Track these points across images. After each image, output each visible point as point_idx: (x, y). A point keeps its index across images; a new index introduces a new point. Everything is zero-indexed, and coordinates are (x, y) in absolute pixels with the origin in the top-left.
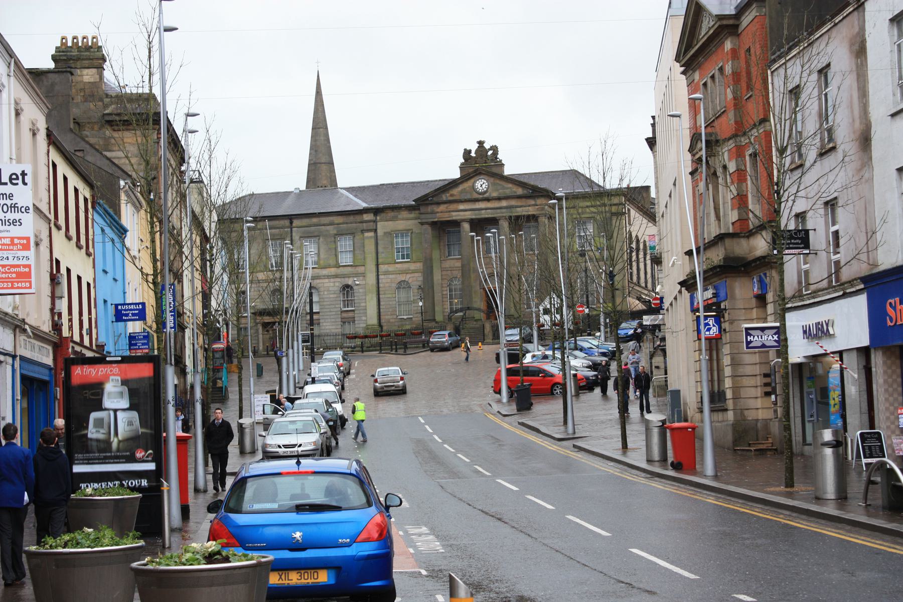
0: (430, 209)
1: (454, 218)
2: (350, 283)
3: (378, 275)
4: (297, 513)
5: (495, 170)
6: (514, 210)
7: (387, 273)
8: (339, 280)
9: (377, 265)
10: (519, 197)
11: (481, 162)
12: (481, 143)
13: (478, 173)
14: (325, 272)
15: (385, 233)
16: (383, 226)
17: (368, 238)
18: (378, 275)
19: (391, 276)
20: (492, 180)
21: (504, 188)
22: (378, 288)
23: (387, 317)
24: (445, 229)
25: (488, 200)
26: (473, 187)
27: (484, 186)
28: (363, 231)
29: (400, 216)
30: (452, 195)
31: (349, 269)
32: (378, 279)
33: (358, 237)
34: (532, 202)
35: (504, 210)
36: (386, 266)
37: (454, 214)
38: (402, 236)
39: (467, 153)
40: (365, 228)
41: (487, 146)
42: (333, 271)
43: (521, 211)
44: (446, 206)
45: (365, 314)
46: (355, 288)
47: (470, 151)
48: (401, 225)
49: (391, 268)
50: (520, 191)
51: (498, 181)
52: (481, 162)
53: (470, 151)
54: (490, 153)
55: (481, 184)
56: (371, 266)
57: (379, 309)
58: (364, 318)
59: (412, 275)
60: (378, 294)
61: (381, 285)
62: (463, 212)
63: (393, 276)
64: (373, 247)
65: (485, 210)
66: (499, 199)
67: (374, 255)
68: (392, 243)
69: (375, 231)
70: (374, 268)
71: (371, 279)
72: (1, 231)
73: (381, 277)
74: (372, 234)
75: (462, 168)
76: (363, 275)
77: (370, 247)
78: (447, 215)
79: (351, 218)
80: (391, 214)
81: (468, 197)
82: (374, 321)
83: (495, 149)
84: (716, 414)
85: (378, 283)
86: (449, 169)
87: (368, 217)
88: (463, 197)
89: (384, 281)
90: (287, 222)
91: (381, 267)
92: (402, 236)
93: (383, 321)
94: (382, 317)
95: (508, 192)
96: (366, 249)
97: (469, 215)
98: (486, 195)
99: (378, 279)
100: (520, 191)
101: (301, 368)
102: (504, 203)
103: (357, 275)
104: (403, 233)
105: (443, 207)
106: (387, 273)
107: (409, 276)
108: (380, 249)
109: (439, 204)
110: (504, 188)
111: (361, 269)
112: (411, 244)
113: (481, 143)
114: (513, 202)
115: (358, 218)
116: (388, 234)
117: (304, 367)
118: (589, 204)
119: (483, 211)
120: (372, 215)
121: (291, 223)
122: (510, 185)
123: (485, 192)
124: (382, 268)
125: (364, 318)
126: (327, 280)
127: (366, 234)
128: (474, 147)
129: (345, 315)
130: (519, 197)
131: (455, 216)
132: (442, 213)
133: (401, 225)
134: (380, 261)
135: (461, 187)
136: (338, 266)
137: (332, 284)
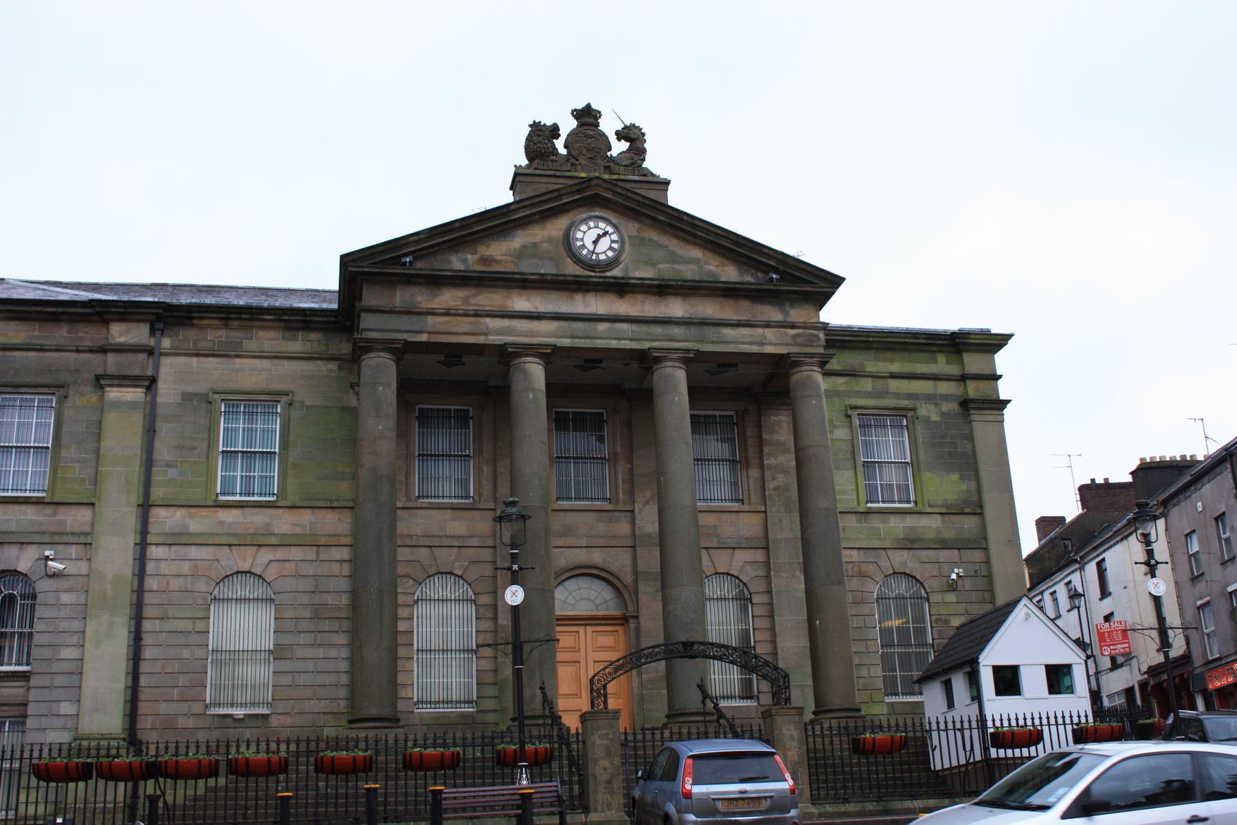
0: (401, 297)
1: (493, 339)
2: (23, 566)
3: (143, 545)
6: (710, 332)
7: (178, 539)
9: (145, 507)
10: (730, 292)
11: (582, 170)
12: (587, 117)
15: (187, 397)
16: (178, 374)
17: (117, 405)
18: (143, 545)
19: (194, 552)
20: (631, 227)
21: (673, 258)
22: (140, 591)
23: (164, 708)
24: (456, 392)
25: (621, 288)
26: (567, 240)
27: (604, 244)
28: (100, 381)
29: (250, 345)
31: (29, 513)
32: (142, 560)
33: (82, 400)
34: (773, 314)
35: (677, 331)
36: (179, 513)
37: (493, 323)
38: (250, 414)
39: (540, 138)
40: (111, 370)
41: (609, 126)
43: (740, 341)
44: (461, 293)
45: (76, 692)
46: (43, 586)
48: (250, 373)
49: (198, 523)
50: (730, 273)
51: (653, 235)
53: (554, 131)
54: (619, 147)
55: (596, 238)
56: (119, 507)
57: (135, 674)
58: (66, 708)
59: (280, 554)
60: (138, 618)
61: (151, 583)
62: (527, 322)
64: (135, 441)
65: (608, 322)
66: (661, 289)
67: (136, 468)
68: (211, 431)
69: (151, 384)
70: (130, 518)
71: (115, 555)
72: (114, 823)
73: (154, 552)
74: (135, 394)
75: (519, 179)
76: (85, 541)
77: (122, 438)
78: (464, 324)
79: (62, 333)
80: (216, 335)
81: (547, 269)
83: (632, 135)
85: (141, 574)
86: (549, 123)
88: (528, 267)
89: (165, 568)
92: (250, 414)
93: (144, 722)
94: (143, 708)
95: (689, 272)
96: (105, 443)
97: (546, 333)
98: (616, 272)
99: (142, 560)
100: (730, 273)
102: (676, 308)
103: (57, 538)
104: (254, 402)
105: (449, 298)
106: (178, 539)
107: (265, 556)
108: (162, 452)
109: (437, 281)
110: (673, 258)
111: (77, 518)
112: (284, 444)
113: (587, 117)
114: (709, 309)
115: (89, 335)
116: (202, 402)
118: (895, 367)
119: (602, 327)
120: (145, 329)
122: (696, 253)
123: (611, 263)
124: (165, 519)
125: (66, 708)
127: (113, 394)
130: (730, 292)
131: (497, 332)
132: (447, 317)
133: (250, 373)
134: (157, 493)
135: (519, 240)
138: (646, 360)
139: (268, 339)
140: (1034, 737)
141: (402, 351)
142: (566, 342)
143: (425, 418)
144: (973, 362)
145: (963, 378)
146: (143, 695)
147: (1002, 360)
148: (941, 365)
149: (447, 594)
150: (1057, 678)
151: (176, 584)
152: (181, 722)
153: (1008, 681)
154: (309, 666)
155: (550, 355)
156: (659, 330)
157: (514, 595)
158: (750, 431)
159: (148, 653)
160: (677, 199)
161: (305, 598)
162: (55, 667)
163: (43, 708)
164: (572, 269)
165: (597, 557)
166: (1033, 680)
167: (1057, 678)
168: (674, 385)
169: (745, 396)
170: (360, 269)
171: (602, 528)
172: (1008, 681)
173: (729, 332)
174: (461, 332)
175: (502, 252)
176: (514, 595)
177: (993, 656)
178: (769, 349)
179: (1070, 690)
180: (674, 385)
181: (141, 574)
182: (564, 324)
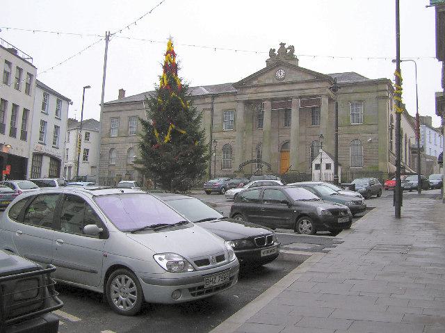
5: (292, 62)
10: (307, 82)
11: (283, 58)
12: (282, 45)
25: (284, 84)
39: (272, 51)
41: (286, 46)
43: (308, 92)
47: (274, 50)
50: (309, 78)
52: (283, 58)
55: (281, 74)
65: (281, 92)
83: (292, 48)
88: (267, 82)
98: (284, 81)
113: (282, 45)
123: (284, 78)
128: (277, 48)
130: (307, 82)
169: (311, 108)
173: (306, 91)
175: (264, 80)
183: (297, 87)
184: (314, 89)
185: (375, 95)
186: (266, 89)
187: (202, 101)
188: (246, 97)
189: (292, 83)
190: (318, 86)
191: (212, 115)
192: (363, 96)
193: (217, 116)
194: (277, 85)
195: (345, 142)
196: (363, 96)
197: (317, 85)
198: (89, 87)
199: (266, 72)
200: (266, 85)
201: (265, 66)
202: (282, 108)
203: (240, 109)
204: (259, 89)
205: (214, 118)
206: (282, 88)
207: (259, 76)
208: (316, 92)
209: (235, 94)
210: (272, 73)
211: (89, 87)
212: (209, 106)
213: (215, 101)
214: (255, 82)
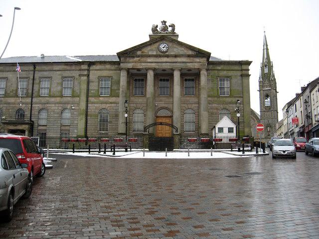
4: (210, 54)
5: (174, 38)
7: (93, 103)
8: (62, 105)
10: (189, 56)
11: (163, 36)
13: (162, 39)
14: (53, 100)
19: (96, 105)
22: (87, 112)
25: (168, 56)
27: (165, 49)
30: (142, 52)
31: (69, 98)
32: (87, 107)
39: (155, 29)
41: (168, 24)
42: (58, 99)
43: (190, 66)
47: (157, 26)
48: (105, 73)
50: (190, 52)
52: (163, 36)
55: (163, 47)
61: (89, 110)
62: (150, 63)
63: (98, 105)
65: (165, 64)
73: (89, 105)
74: (85, 78)
81: (155, 53)
82: (83, 134)
83: (173, 26)
84: (34, 133)
85: (87, 109)
87: (85, 67)
88: (150, 53)
90: (32, 68)
91: (90, 98)
95: (181, 53)
98: (167, 53)
99: (87, 107)
100: (190, 52)
101: (230, 150)
106: (93, 103)
107: (108, 105)
114: (184, 59)
117: (230, 148)
121: (35, 68)
123: (166, 52)
124: (91, 99)
126: (53, 105)
127: (82, 78)
128: (160, 26)
129: (63, 128)
130: (189, 56)
134: (90, 95)
136: (62, 96)
137: (56, 108)
138: (173, 70)
139: (108, 66)
140: (221, 140)
141: (128, 70)
142: (157, 67)
143: (186, 80)
144: (244, 67)
145: (242, 70)
146: (88, 129)
147: (250, 67)
148: (237, 67)
149: (139, 112)
150: (230, 130)
151: (93, 110)
152: (94, 134)
153: (221, 130)
154: (115, 124)
155: (154, 70)
156: (174, 64)
157: (126, 115)
158: (197, 82)
159: (88, 122)
160: (180, 39)
161: (114, 113)
162: (74, 124)
163: (72, 131)
164: (159, 53)
165: (166, 106)
166: (226, 130)
167: (230, 130)
168: (150, 75)
169: (190, 77)
170: (121, 55)
171: (167, 100)
172: (221, 130)
173: (188, 64)
174: (139, 66)
175: (146, 50)
176: (126, 115)
177: (218, 126)
178: (196, 67)
179: (233, 132)
180: (150, 75)
181: (87, 109)
182: (157, 64)
183: (179, 60)
184: (196, 64)
185: (239, 73)
186: (149, 60)
187: (78, 68)
188: (130, 66)
189: (176, 56)
190: (198, 60)
191: (88, 83)
192: (230, 73)
193: (93, 82)
194: (160, 56)
195: (215, 111)
196: (230, 73)
197: (197, 60)
198: (19, 9)
199: (151, 44)
200: (150, 56)
201: (147, 39)
202: (164, 77)
203: (123, 78)
204: (143, 59)
205: (91, 84)
206: (165, 59)
207: (144, 47)
208: (197, 66)
209: (118, 63)
210: (156, 45)
211: (19, 9)
212: (86, 73)
213: (91, 68)
214: (139, 53)
